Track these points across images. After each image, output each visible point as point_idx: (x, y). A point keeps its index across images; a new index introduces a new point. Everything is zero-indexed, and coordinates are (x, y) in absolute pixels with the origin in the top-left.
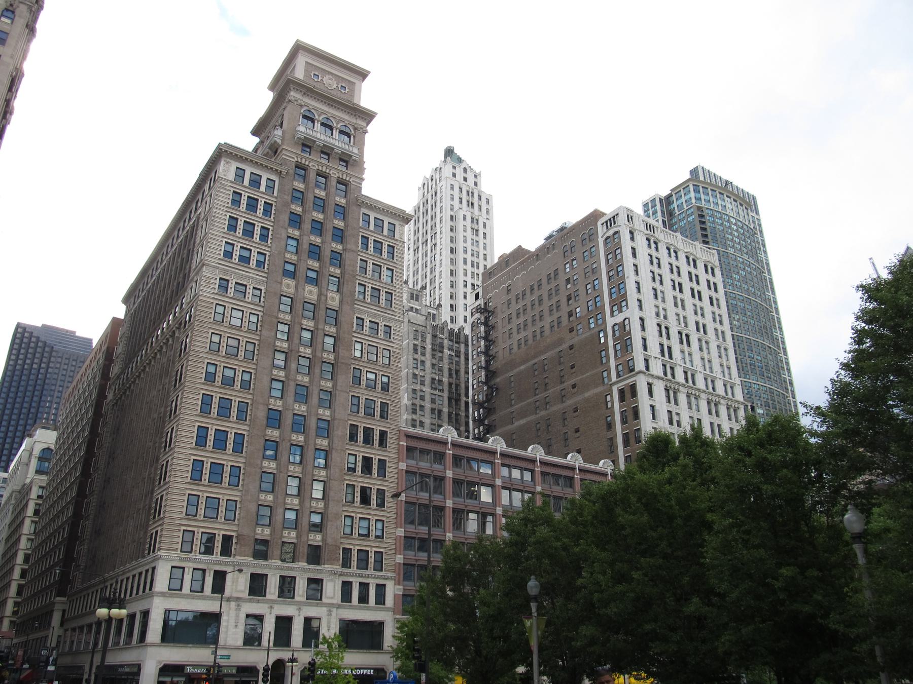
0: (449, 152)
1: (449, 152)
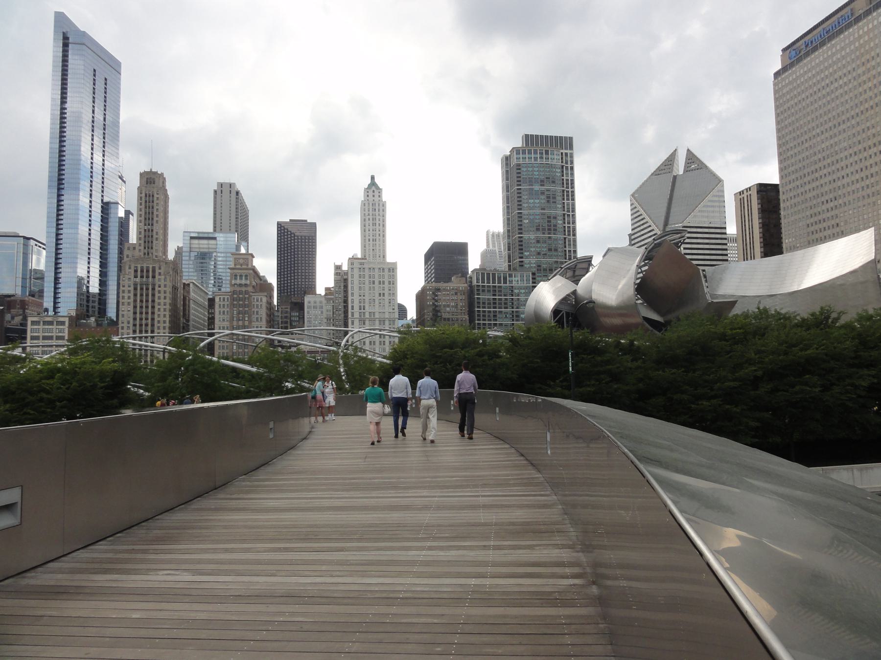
0: (373, 178)
1: (373, 178)
